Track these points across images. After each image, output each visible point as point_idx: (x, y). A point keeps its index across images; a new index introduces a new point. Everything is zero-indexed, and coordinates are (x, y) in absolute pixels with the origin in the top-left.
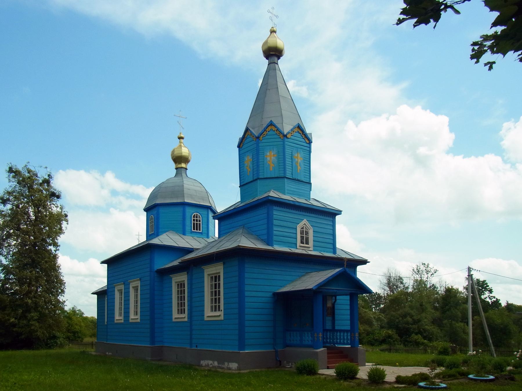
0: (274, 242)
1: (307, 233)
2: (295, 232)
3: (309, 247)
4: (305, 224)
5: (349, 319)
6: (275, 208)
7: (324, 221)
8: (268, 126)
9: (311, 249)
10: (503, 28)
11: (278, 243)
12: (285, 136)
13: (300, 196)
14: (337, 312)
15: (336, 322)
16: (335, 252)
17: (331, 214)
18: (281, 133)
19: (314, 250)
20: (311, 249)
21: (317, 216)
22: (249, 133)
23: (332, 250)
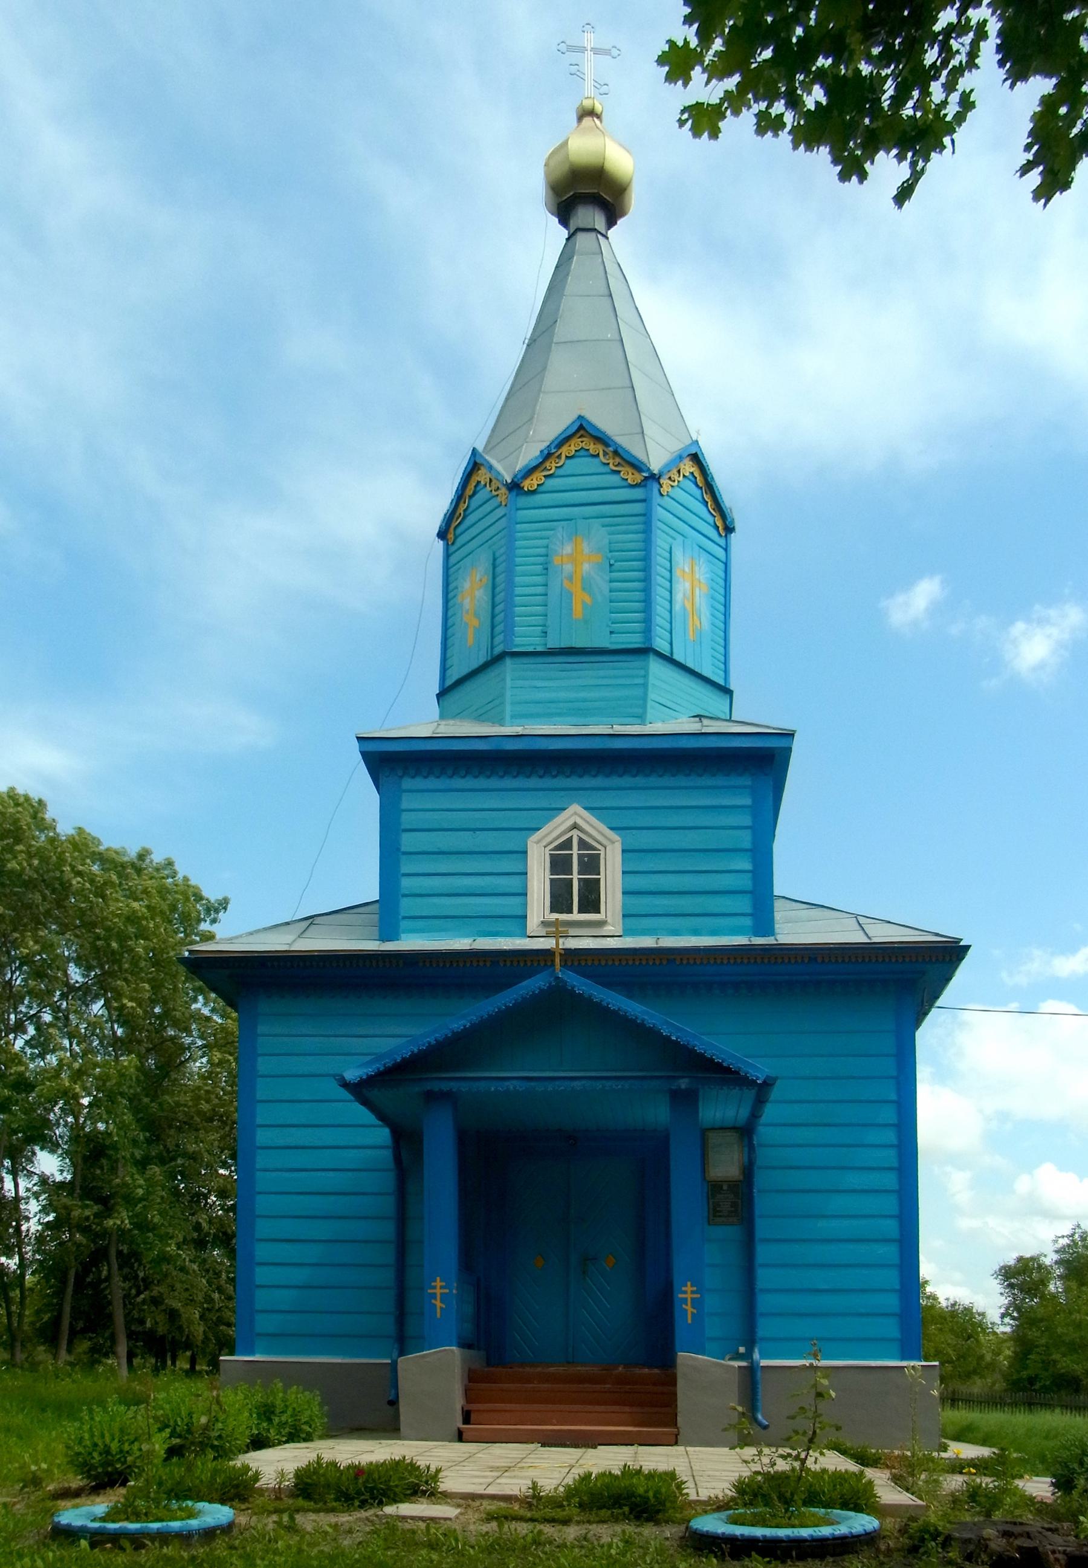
0: (404, 924)
1: (591, 864)
2: (518, 868)
3: (601, 924)
4: (575, 826)
5: (896, 1260)
6: (407, 783)
7: (715, 807)
8: (564, 440)
9: (608, 929)
10: (1041, 168)
11: (421, 923)
12: (655, 478)
13: (550, 715)
14: (762, 1204)
15: (763, 1253)
16: (763, 920)
17: (758, 763)
18: (636, 466)
19: (628, 932)
20: (608, 929)
21: (640, 781)
22: (482, 476)
23: (744, 904)
